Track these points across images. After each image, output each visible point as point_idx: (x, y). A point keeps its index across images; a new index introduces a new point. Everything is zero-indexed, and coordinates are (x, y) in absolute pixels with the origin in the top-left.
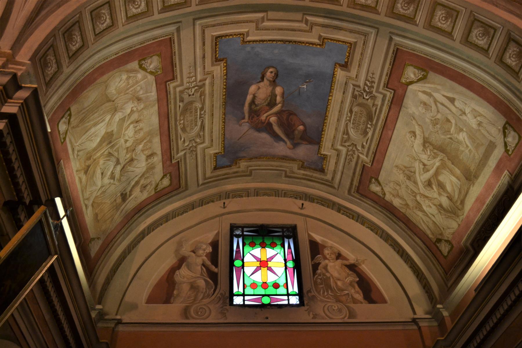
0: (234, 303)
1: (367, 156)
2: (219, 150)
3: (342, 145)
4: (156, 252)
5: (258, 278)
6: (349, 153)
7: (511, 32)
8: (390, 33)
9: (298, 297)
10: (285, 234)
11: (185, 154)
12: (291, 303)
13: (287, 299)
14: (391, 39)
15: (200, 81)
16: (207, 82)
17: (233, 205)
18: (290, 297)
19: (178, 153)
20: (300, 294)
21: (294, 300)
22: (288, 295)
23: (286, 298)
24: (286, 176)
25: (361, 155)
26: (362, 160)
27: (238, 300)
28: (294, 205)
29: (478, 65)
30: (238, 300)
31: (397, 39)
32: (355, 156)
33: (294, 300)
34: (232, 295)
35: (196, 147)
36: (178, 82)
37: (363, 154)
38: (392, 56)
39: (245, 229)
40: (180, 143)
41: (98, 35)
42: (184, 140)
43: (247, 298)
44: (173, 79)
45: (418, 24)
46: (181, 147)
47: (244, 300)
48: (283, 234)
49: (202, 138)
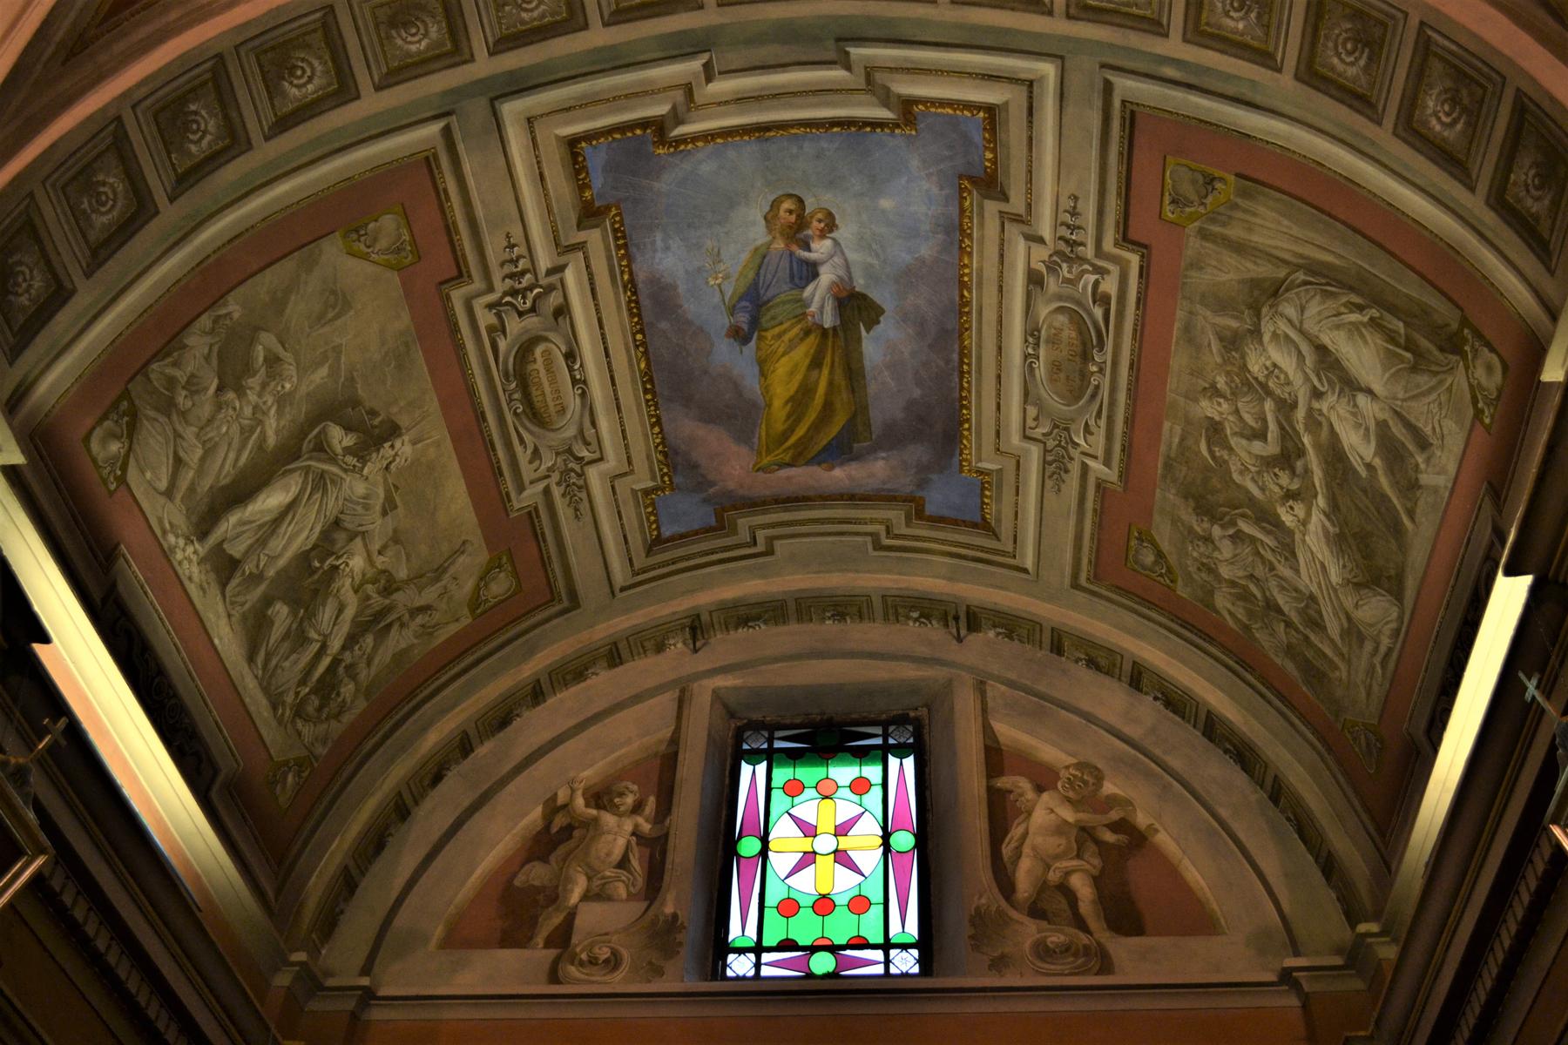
0: (729, 973)
1: (1107, 463)
2: (653, 478)
3: (1026, 437)
4: (1539, 983)
5: (806, 885)
6: (1049, 458)
7: (491, 45)
8: (1103, 66)
9: (915, 952)
10: (891, 741)
11: (547, 492)
12: (893, 970)
13: (882, 959)
14: (1108, 88)
15: (550, 272)
16: (570, 276)
17: (725, 646)
18: (893, 953)
19: (521, 488)
20: (926, 944)
21: (905, 962)
22: (887, 946)
23: (878, 955)
24: (878, 546)
25: (1090, 462)
26: (1097, 478)
27: (740, 966)
28: (912, 635)
29: (367, 135)
30: (740, 966)
31: (1126, 86)
32: (1075, 468)
33: (905, 962)
34: (721, 948)
35: (581, 475)
36: (478, 284)
37: (1095, 457)
38: (1122, 137)
39: (779, 734)
40: (523, 457)
41: (185, 180)
42: (536, 452)
43: (766, 957)
44: (460, 275)
45: (216, 56)
46: (526, 477)
47: (758, 965)
48: (885, 740)
49: (594, 446)
